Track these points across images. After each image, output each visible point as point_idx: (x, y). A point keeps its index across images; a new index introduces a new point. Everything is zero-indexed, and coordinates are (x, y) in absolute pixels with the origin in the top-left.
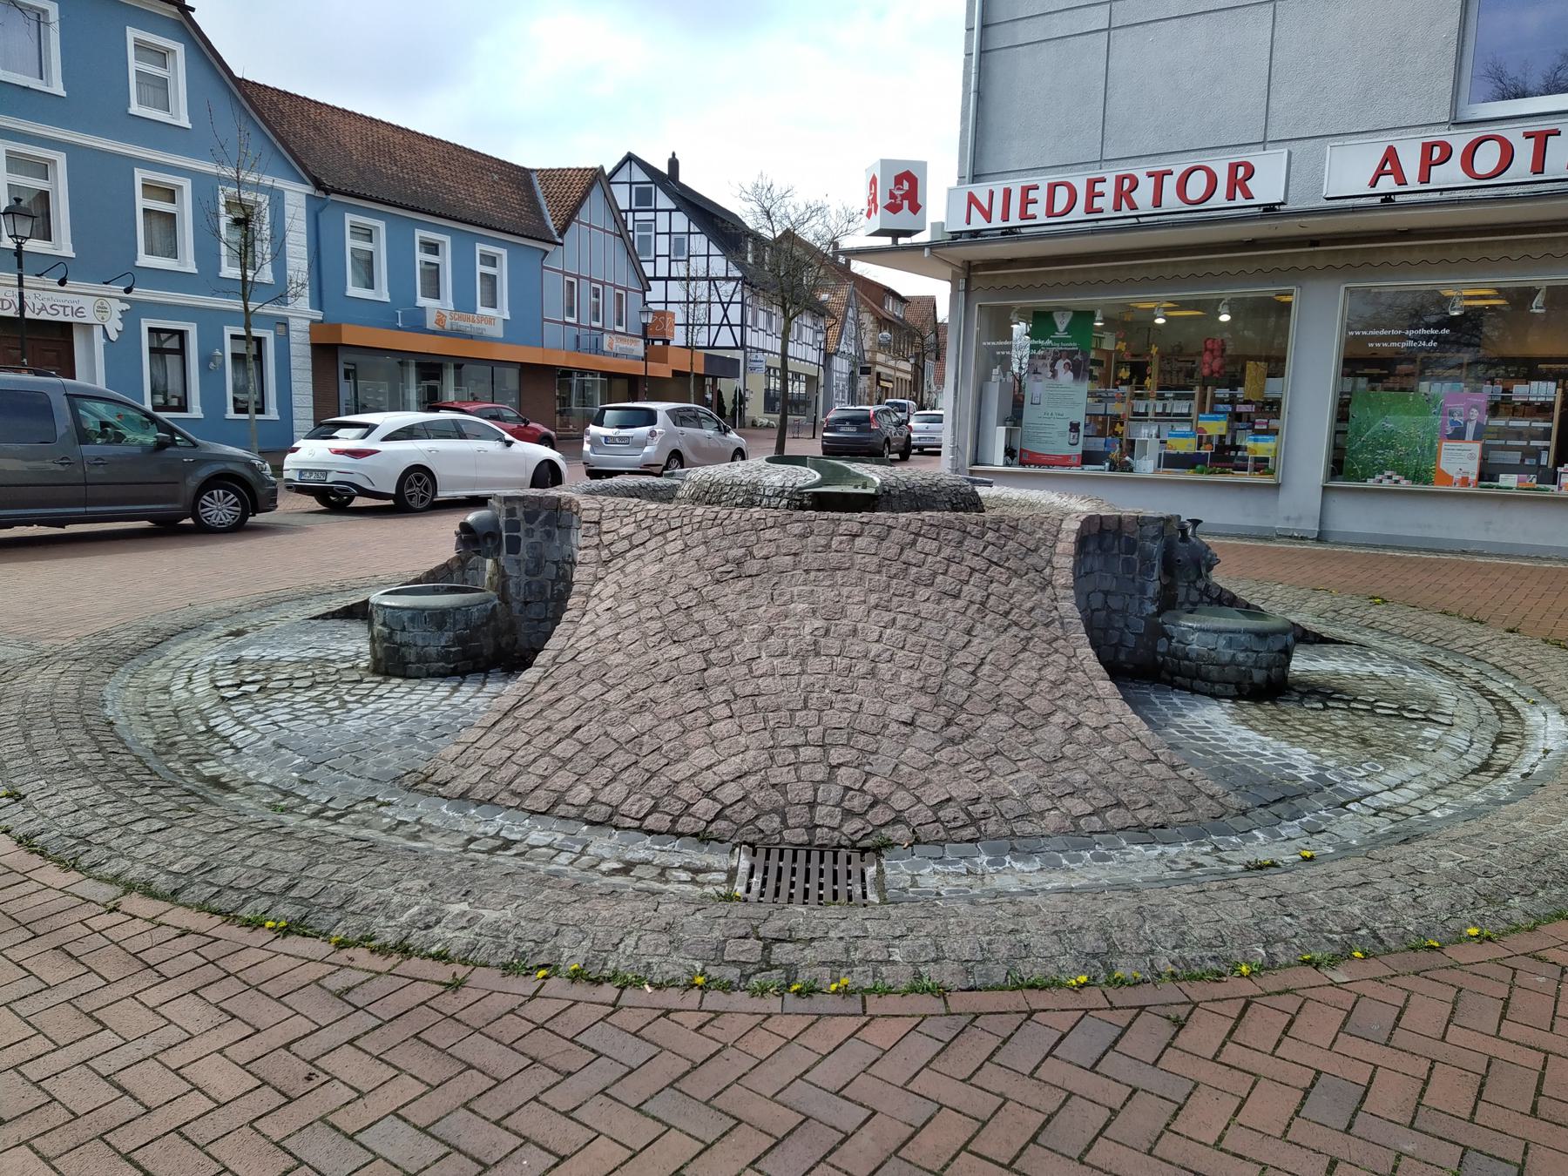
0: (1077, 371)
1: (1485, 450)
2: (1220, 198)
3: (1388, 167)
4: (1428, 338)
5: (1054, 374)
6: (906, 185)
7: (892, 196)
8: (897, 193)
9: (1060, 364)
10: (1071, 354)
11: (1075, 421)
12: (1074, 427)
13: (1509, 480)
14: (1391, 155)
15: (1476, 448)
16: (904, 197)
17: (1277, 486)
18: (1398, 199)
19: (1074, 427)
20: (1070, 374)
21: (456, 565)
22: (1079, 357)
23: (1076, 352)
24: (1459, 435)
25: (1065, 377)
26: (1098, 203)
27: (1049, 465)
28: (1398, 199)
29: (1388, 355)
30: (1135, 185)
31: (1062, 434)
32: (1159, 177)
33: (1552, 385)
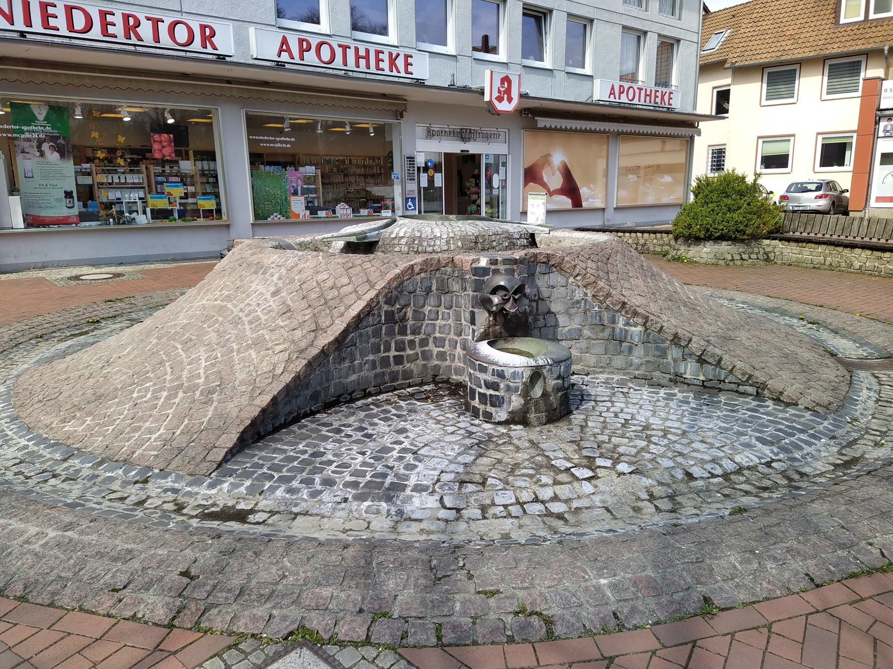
0: (63, 152)
1: (306, 198)
2: (197, 45)
3: (284, 47)
4: (286, 142)
5: (42, 154)
6: (506, 85)
7: (499, 91)
8: (502, 89)
9: (45, 147)
10: (52, 138)
11: (69, 189)
12: (68, 195)
13: (322, 214)
14: (284, 41)
15: (302, 198)
16: (505, 92)
17: (228, 226)
18: (287, 66)
19: (68, 195)
20: (56, 155)
21: (333, 348)
22: (61, 141)
23: (59, 138)
24: (295, 193)
25: (53, 157)
26: (111, 30)
27: (44, 225)
28: (287, 66)
29: (279, 151)
30: (138, 24)
31: (58, 200)
32: (156, 22)
33: (314, 168)
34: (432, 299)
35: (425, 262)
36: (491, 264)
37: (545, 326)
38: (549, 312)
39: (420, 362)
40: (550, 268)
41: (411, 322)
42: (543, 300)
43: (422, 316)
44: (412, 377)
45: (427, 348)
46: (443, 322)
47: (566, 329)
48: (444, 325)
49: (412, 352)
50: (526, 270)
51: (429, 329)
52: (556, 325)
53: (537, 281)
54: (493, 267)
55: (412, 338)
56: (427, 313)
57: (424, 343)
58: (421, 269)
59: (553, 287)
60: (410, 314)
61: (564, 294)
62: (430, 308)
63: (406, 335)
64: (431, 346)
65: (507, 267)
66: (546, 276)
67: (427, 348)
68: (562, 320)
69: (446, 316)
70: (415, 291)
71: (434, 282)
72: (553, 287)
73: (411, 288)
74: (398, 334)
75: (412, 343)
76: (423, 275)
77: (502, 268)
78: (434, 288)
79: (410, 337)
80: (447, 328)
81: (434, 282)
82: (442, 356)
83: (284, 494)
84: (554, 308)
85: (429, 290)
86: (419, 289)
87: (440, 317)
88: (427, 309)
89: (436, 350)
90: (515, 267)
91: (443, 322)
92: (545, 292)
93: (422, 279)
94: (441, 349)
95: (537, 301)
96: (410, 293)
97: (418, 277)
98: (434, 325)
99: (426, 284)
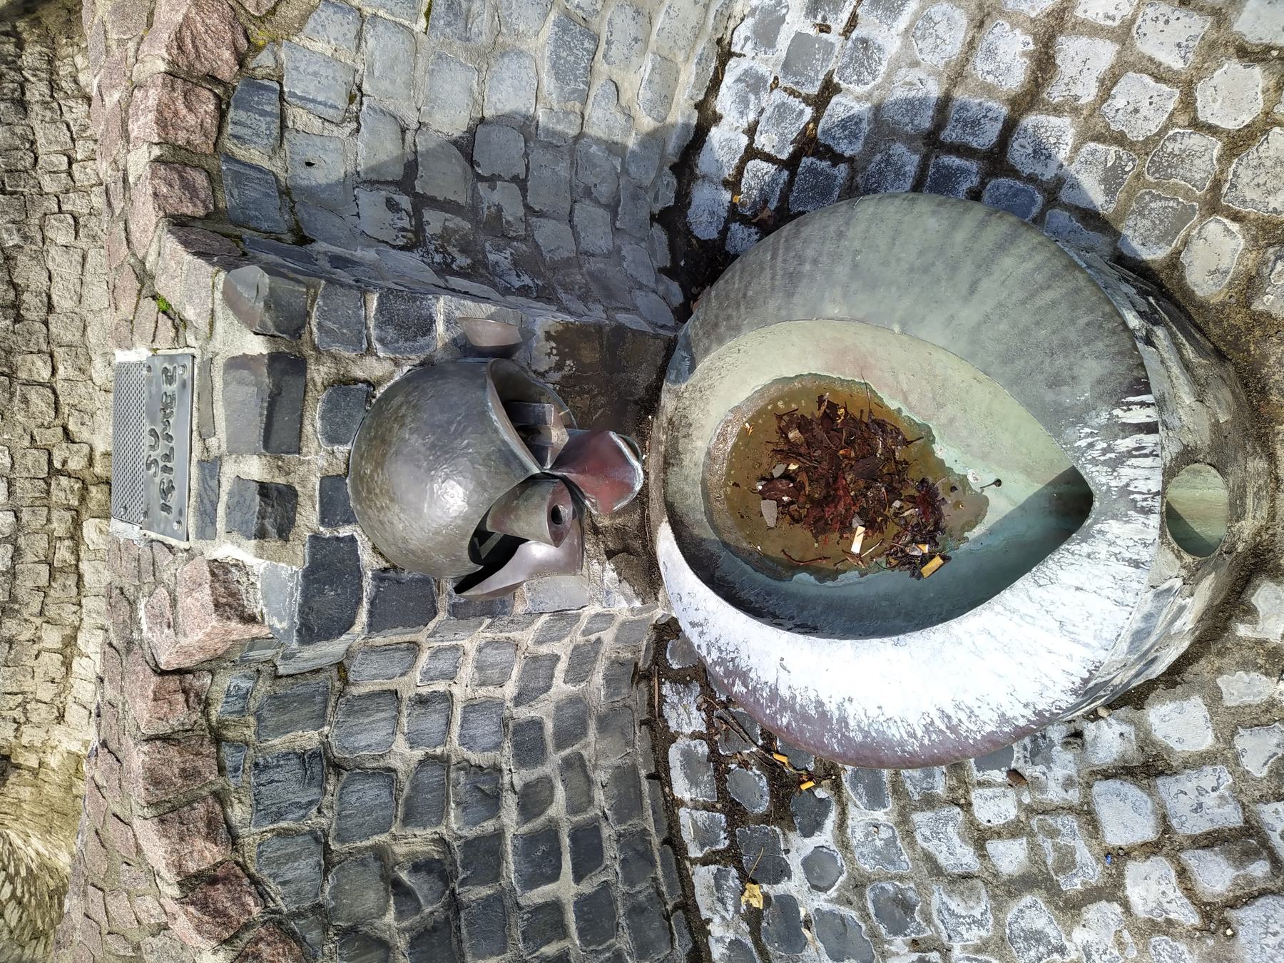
34: (363, 740)
35: (168, 812)
36: (284, 530)
37: (521, 184)
38: (466, 146)
39: (591, 744)
40: (253, 83)
41: (454, 824)
42: (411, 167)
43: (431, 776)
44: (634, 769)
45: (549, 727)
46: (467, 672)
47: (548, 83)
48: (480, 667)
49: (560, 793)
50: (345, 301)
51: (485, 728)
52: (525, 126)
53: (318, 177)
54: (308, 517)
55: (510, 803)
56: (418, 754)
57: (528, 743)
58: (211, 836)
59: (356, 95)
60: (414, 842)
61: (397, 43)
62: (400, 745)
63: (499, 835)
64: (542, 710)
65: (314, 422)
66: (299, 117)
67: (549, 727)
68: (507, 96)
69: (443, 664)
70: (319, 838)
71: (278, 743)
72: (356, 95)
73: (305, 867)
74: (497, 877)
75: (532, 799)
76: (238, 813)
77: (318, 458)
78: (308, 738)
79: (510, 815)
80: (492, 656)
81: (278, 743)
82: (582, 661)
83: (617, 828)
84: (451, 120)
85: (322, 765)
86: (315, 820)
87: (441, 686)
88: (404, 755)
89: (561, 687)
90: (319, 373)
91: (467, 672)
92: (375, 148)
93: (264, 811)
94: (562, 666)
95: (422, 202)
96: (328, 864)
97: (250, 836)
98: (471, 707)
99: (287, 785)
